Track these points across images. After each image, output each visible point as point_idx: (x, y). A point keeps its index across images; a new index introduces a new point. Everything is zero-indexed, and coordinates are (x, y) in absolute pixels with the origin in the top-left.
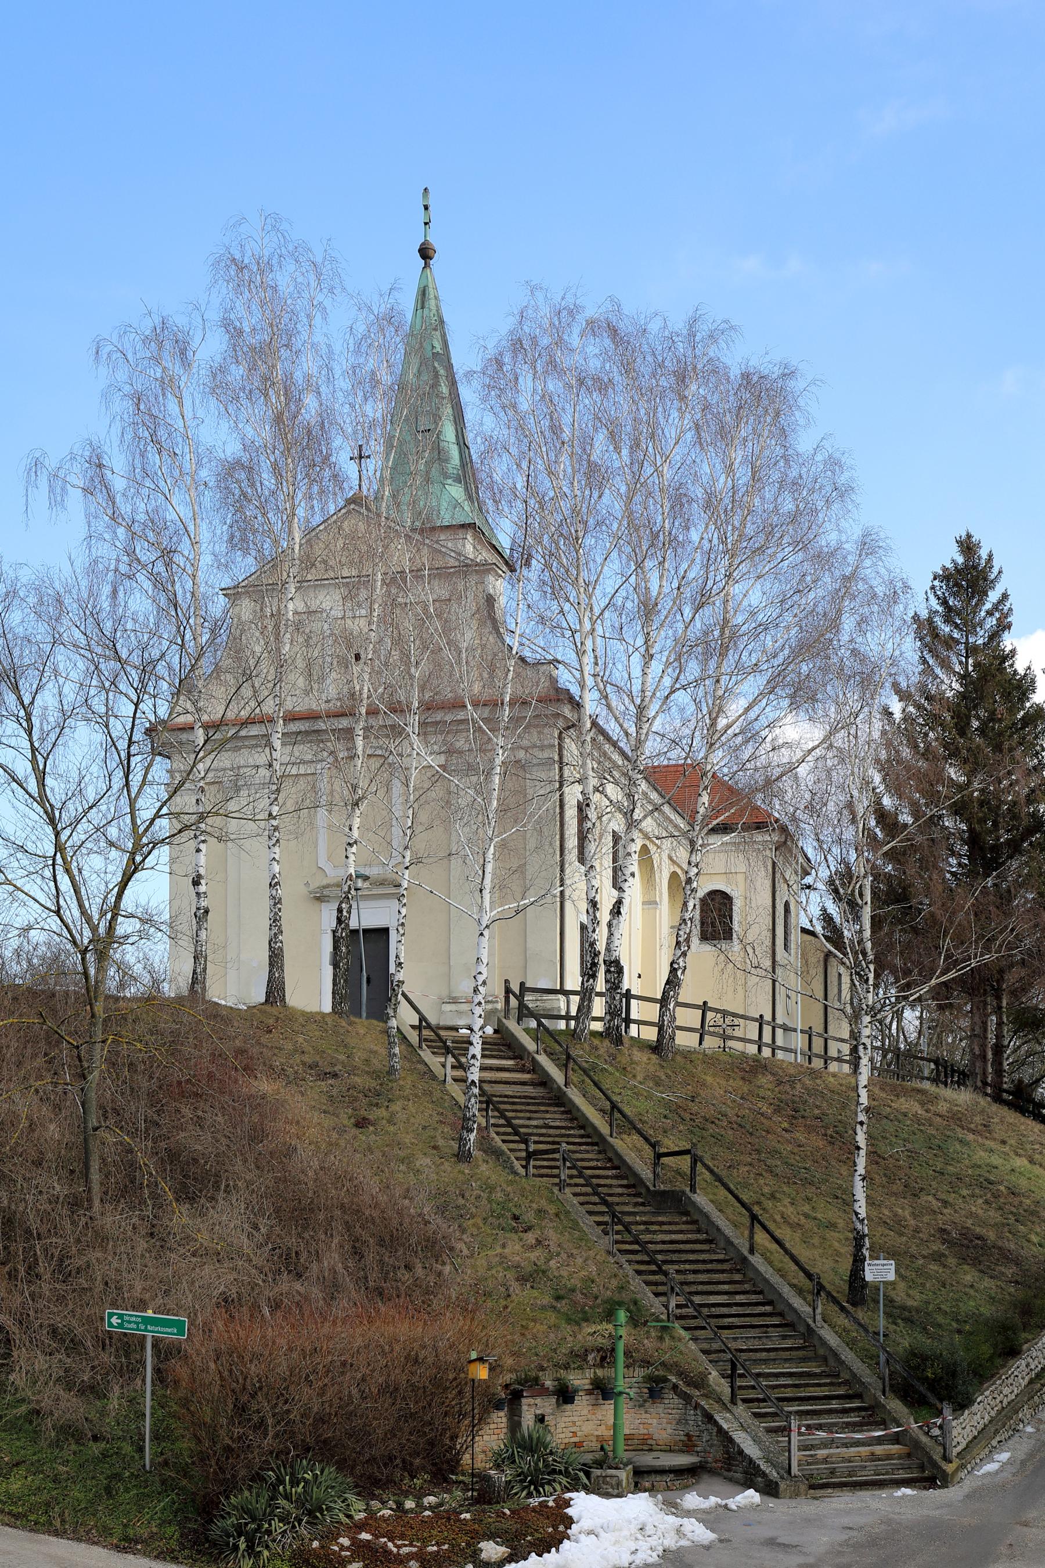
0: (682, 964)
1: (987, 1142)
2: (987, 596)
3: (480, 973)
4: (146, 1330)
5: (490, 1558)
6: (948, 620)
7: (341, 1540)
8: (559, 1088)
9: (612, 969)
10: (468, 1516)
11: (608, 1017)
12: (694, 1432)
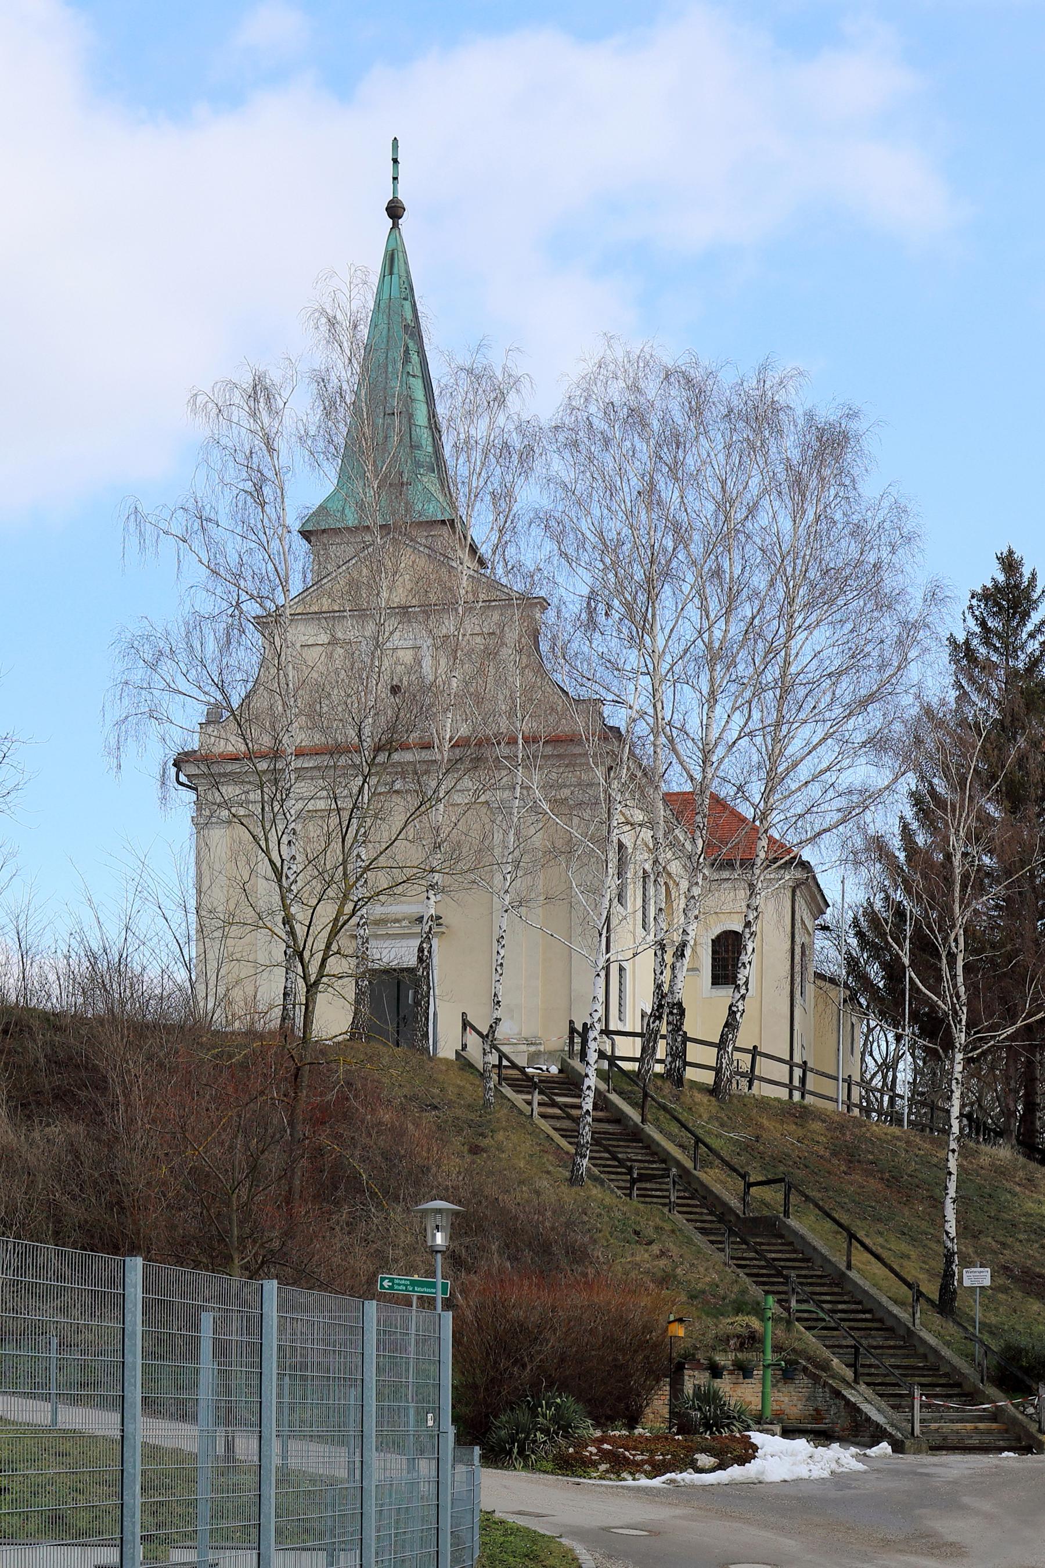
0: (741, 1008)
1: (1035, 1195)
2: (1029, 617)
3: (596, 1011)
4: (413, 1291)
5: (705, 1465)
6: (987, 643)
7: (589, 1448)
8: (636, 1124)
9: (675, 1011)
10: (680, 1437)
11: (669, 1059)
12: (822, 1407)
